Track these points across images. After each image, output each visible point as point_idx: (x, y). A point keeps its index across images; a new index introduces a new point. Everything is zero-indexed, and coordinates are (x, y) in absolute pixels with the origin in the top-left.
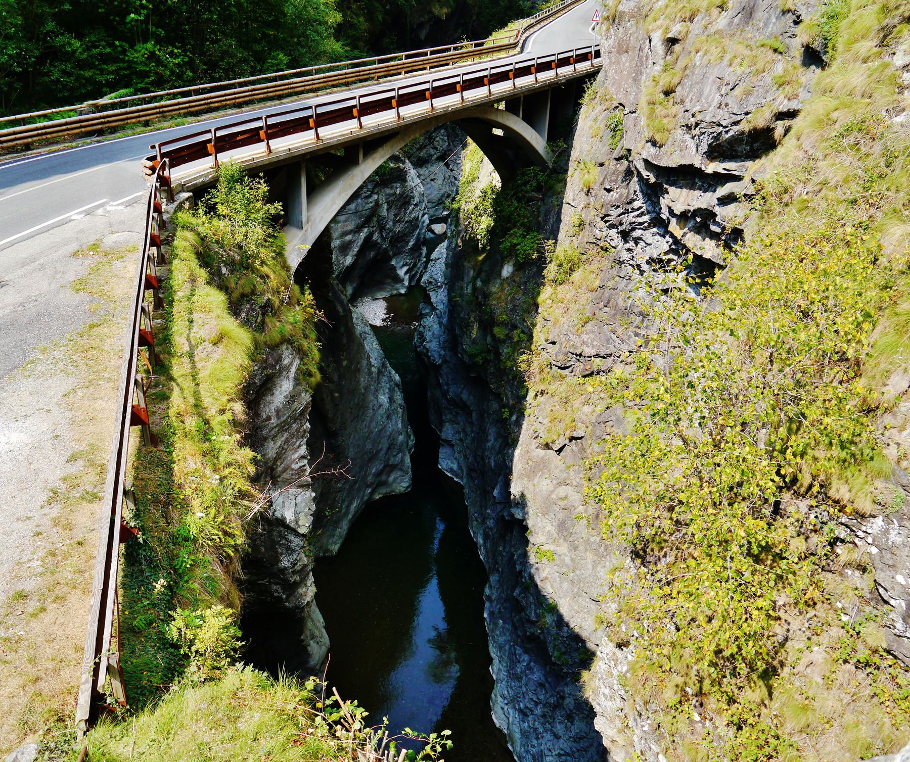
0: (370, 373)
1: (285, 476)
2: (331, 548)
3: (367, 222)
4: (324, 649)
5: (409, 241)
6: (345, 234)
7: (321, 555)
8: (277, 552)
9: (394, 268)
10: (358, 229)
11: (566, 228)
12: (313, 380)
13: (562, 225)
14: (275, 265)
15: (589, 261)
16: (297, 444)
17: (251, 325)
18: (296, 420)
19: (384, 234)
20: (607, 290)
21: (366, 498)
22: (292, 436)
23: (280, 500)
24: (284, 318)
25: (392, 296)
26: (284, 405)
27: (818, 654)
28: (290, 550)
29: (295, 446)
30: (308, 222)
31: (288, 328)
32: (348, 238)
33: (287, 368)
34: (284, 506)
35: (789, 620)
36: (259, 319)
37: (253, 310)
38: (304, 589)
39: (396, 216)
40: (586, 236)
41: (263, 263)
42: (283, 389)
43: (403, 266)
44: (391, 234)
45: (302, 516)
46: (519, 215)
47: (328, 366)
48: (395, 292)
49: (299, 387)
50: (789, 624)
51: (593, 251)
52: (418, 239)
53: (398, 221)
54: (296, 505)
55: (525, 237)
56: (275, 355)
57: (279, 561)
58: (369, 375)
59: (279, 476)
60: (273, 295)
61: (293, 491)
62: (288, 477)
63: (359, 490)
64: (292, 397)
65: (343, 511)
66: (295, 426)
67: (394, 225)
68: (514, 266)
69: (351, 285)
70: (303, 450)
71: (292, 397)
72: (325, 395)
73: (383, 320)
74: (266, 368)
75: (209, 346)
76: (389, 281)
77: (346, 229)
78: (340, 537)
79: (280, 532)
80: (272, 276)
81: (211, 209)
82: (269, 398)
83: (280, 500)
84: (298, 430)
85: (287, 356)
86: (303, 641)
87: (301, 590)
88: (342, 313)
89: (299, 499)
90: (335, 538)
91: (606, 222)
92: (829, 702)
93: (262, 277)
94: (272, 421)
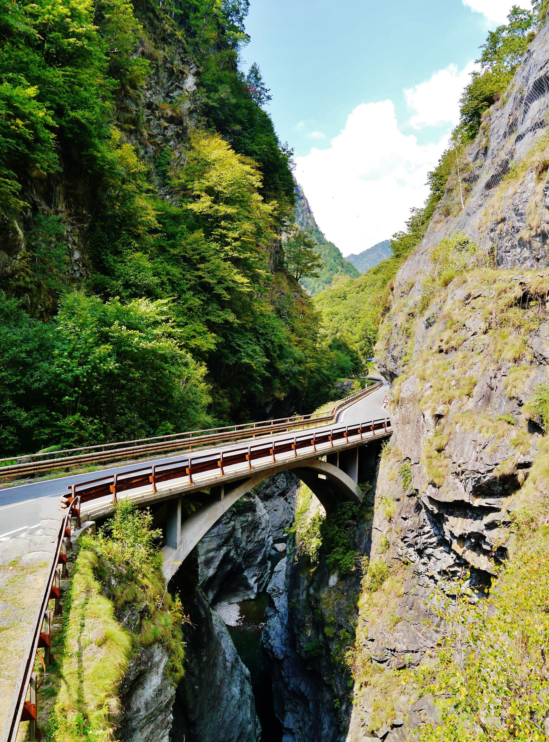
0: (225, 667)
3: (226, 542)
5: (257, 557)
6: (209, 551)
9: (246, 578)
10: (219, 548)
11: (376, 547)
13: (372, 545)
14: (154, 578)
15: (395, 573)
17: (131, 627)
18: (161, 711)
19: (239, 552)
20: (411, 596)
24: (157, 621)
25: (244, 601)
26: (152, 698)
30: (181, 543)
31: (161, 629)
32: (212, 554)
39: (248, 537)
40: (391, 553)
42: (153, 683)
43: (253, 576)
44: (244, 551)
48: (246, 598)
49: (166, 682)
51: (397, 565)
52: (265, 554)
53: (249, 541)
56: (148, 653)
60: (150, 602)
67: (246, 545)
68: (338, 576)
72: (187, 688)
73: (237, 621)
75: (94, 646)
76: (242, 588)
81: (108, 534)
82: (140, 692)
88: (204, 616)
91: (405, 542)
93: (142, 587)
94: (141, 713)
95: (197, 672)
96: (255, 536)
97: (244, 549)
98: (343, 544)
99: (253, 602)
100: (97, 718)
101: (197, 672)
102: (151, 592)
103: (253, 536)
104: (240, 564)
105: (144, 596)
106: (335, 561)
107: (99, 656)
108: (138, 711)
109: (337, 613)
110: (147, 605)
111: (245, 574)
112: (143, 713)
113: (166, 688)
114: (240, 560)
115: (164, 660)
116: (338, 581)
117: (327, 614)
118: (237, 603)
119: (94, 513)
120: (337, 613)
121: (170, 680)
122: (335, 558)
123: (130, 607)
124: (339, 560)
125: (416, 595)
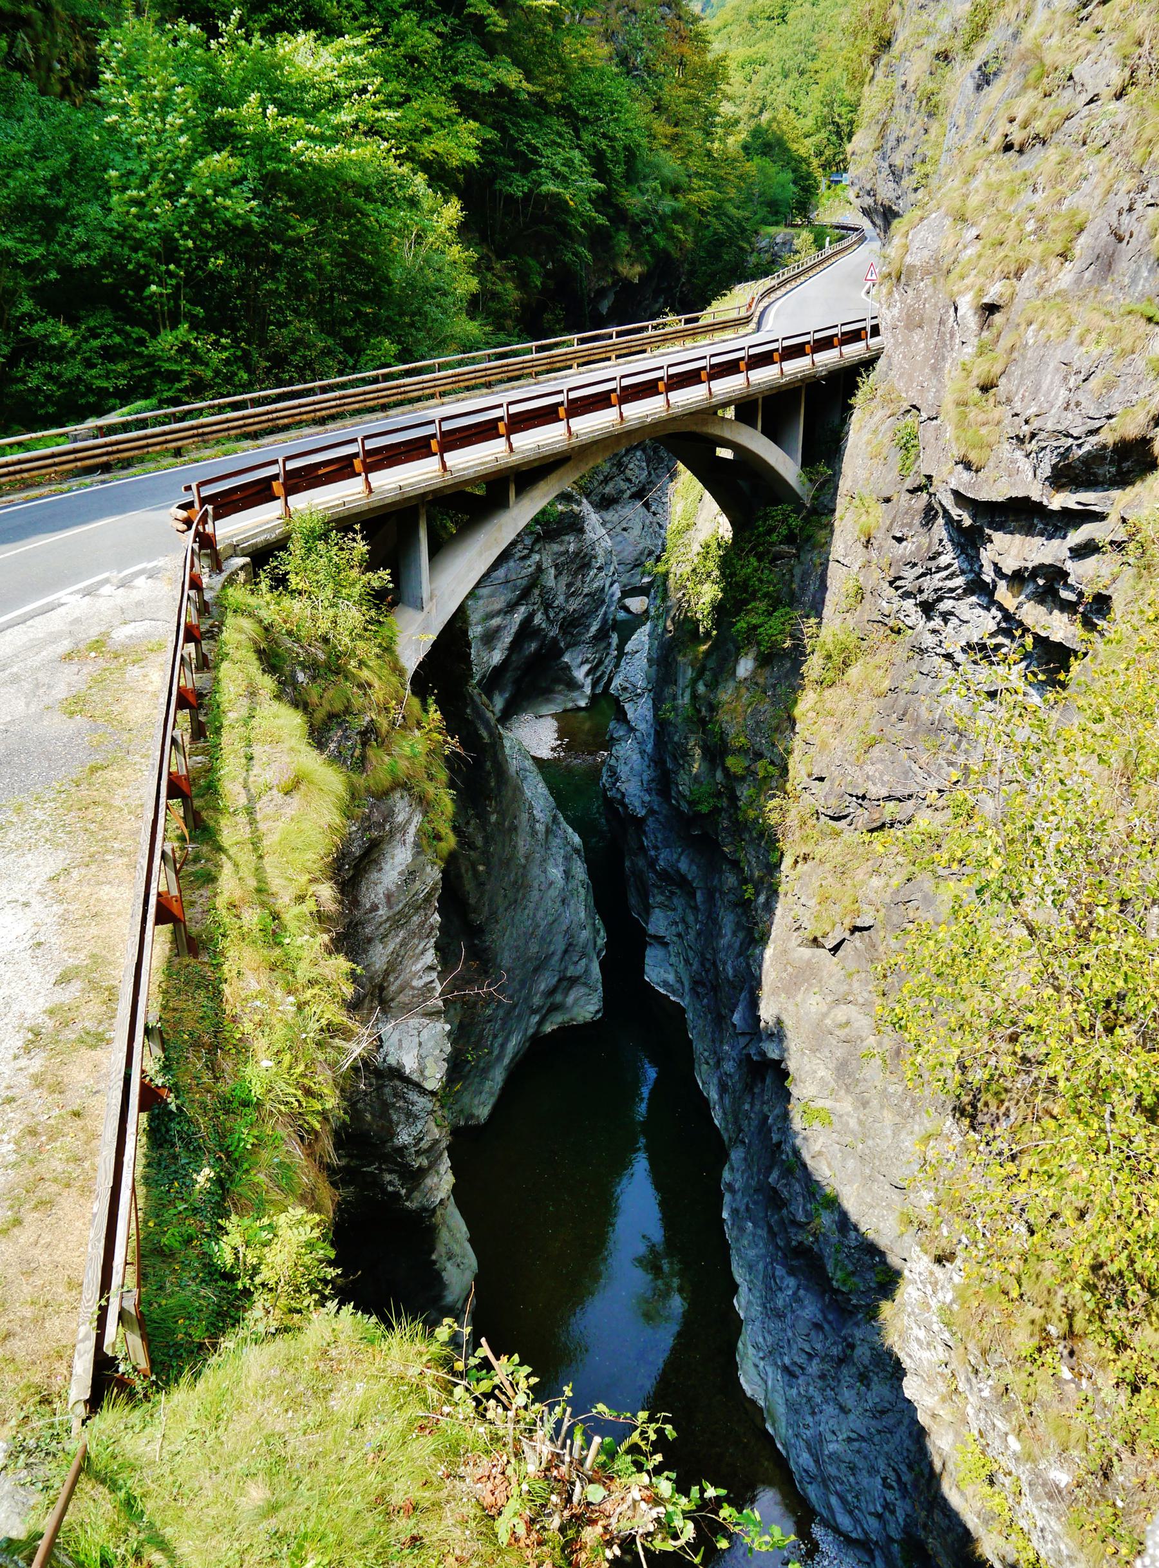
0: (534, 833)
1: (402, 998)
2: (476, 1112)
5: (590, 626)
7: (462, 1123)
8: (391, 1121)
9: (568, 668)
10: (511, 608)
13: (828, 596)
14: (381, 667)
15: (873, 651)
16: (421, 947)
17: (345, 762)
19: (552, 615)
20: (902, 695)
21: (531, 1031)
23: (395, 1037)
24: (396, 750)
25: (565, 711)
26: (398, 886)
30: (431, 599)
31: (403, 764)
32: (495, 622)
33: (403, 829)
34: (400, 1046)
36: (357, 753)
37: (348, 738)
38: (436, 1180)
39: (569, 585)
40: (867, 610)
41: (362, 664)
42: (397, 860)
43: (583, 663)
44: (562, 615)
45: (429, 1062)
46: (760, 580)
47: (468, 823)
48: (570, 705)
49: (422, 858)
53: (573, 594)
54: (420, 1044)
55: (770, 614)
56: (383, 807)
57: (393, 1135)
59: (392, 1000)
61: (414, 1022)
64: (411, 873)
65: (496, 1053)
67: (567, 601)
68: (756, 659)
72: (463, 870)
73: (553, 749)
74: (369, 828)
76: (561, 687)
77: (489, 609)
78: (492, 1094)
79: (394, 1088)
80: (376, 683)
81: (280, 581)
82: (374, 876)
83: (395, 1037)
84: (422, 925)
85: (403, 810)
89: (425, 1034)
90: (484, 1096)
91: (897, 588)
93: (360, 686)
94: (380, 912)
95: (479, 842)
97: (562, 610)
98: (766, 595)
99: (582, 714)
101: (479, 842)
103: (579, 584)
107: (289, 812)
108: (374, 908)
111: (566, 658)
112: (382, 912)
113: (424, 869)
114: (554, 632)
116: (756, 668)
117: (732, 732)
118: (552, 715)
119: (246, 540)
124: (756, 627)
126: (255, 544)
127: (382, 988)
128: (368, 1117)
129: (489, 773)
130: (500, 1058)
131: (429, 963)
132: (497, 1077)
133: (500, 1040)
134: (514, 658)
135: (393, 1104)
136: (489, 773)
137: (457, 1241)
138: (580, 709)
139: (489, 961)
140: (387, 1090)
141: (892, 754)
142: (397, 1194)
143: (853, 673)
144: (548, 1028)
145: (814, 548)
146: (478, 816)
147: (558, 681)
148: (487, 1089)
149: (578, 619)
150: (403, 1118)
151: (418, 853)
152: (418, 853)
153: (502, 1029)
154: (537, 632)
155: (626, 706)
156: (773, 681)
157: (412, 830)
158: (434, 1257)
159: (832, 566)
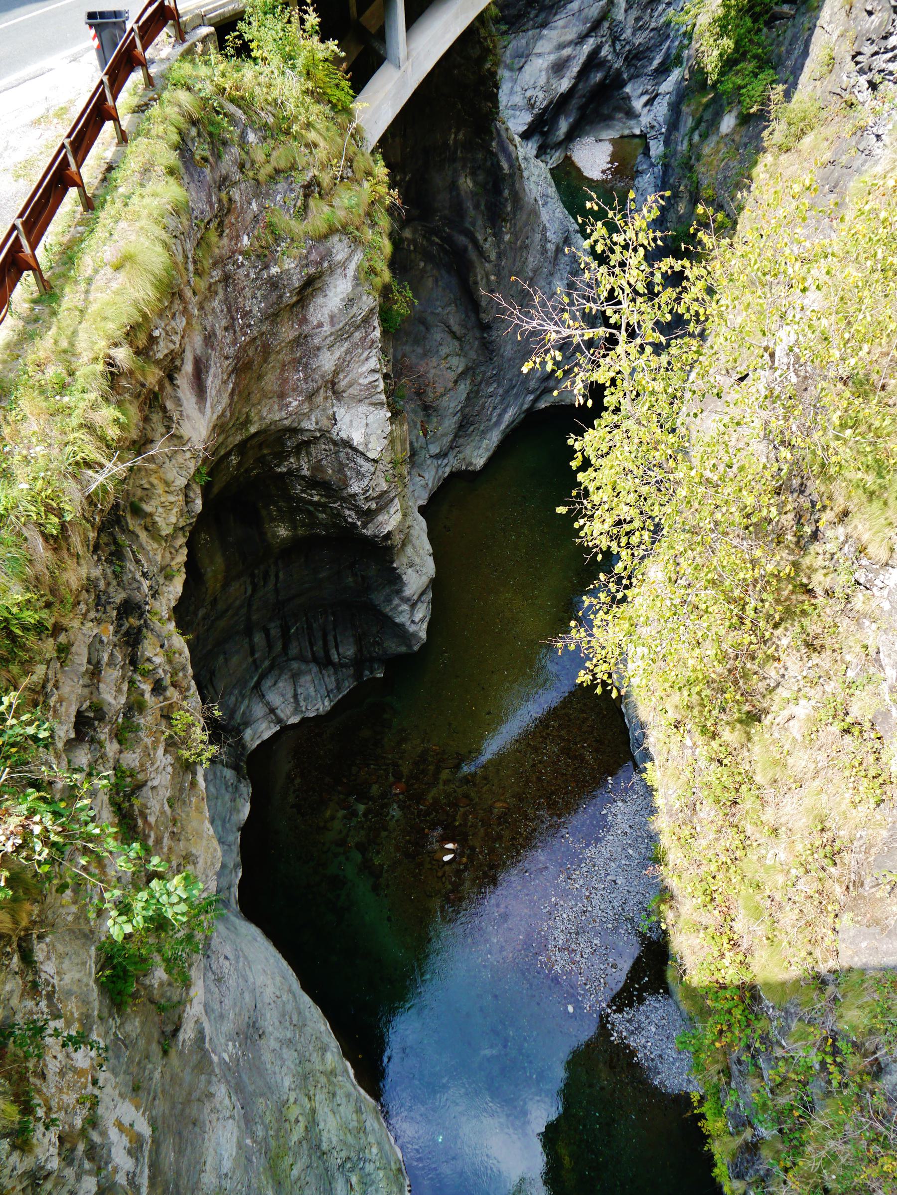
0: (544, 251)
1: (351, 391)
2: (474, 461)
3: (596, 26)
4: (424, 580)
5: (653, 59)
6: (561, 46)
7: (464, 468)
8: (345, 476)
9: (628, 98)
10: (582, 39)
11: (813, 66)
12: (378, 281)
13: (808, 63)
14: (328, 129)
15: (825, 122)
16: (365, 355)
17: (288, 210)
18: (358, 327)
19: (618, 48)
20: (838, 168)
21: (525, 407)
22: (355, 346)
23: (347, 418)
24: (336, 202)
25: (622, 137)
26: (340, 310)
27: (803, 710)
28: (360, 475)
29: (362, 358)
30: (408, 58)
31: (341, 214)
32: (567, 52)
33: (344, 265)
34: (351, 425)
35: (788, 664)
36: (299, 203)
37: (292, 190)
38: (386, 517)
39: (638, 19)
40: (830, 83)
41: (308, 125)
42: (339, 290)
43: (642, 94)
44: (627, 48)
45: (373, 438)
46: (751, 41)
47: (486, 240)
48: (626, 132)
49: (360, 288)
50: (786, 669)
51: (836, 105)
52: (667, 55)
53: (640, 28)
54: (367, 425)
55: (756, 75)
56: (321, 248)
57: (347, 486)
58: (542, 254)
59: (344, 391)
60: (320, 171)
61: (363, 408)
62: (356, 393)
63: (517, 396)
64: (350, 300)
65: (494, 420)
66: (358, 335)
67: (634, 34)
68: (737, 117)
69: (566, 119)
70: (373, 363)
71: (350, 300)
72: (479, 277)
73: (603, 172)
74: (307, 265)
75: (109, 270)
76: (621, 115)
77: (563, 39)
78: (487, 450)
79: (347, 454)
80: (322, 144)
81: (244, 50)
82: (320, 300)
83: (347, 418)
84: (363, 339)
85: (340, 249)
86: (396, 569)
87: (381, 518)
88: (506, 171)
89: (371, 419)
90: (481, 451)
91: (857, 63)
92: (800, 761)
93: (307, 145)
94: (325, 329)
95: (493, 256)
96: (652, 17)
97: (628, 43)
98: (756, 57)
99: (637, 140)
100: (86, 377)
101: (493, 256)
102: (321, 154)
103: (647, 18)
104: (619, 72)
105: (311, 160)
106: (733, 88)
107: (115, 285)
108: (320, 325)
109: (720, 183)
110: (315, 176)
111: (628, 89)
112: (327, 329)
113: (361, 298)
114: (618, 64)
115: (356, 258)
116: (736, 125)
117: (705, 183)
118: (611, 140)
119: (215, 9)
120: (720, 183)
121: (366, 287)
122: (733, 83)
123: (287, 178)
124: (740, 87)
125: (847, 168)
126: (224, 13)
127: (333, 384)
128: (330, 471)
129: (507, 200)
130: (498, 423)
131: (372, 367)
132: (494, 438)
133: (498, 411)
134: (580, 86)
135: (347, 465)
136: (507, 200)
137: (419, 555)
138: (634, 136)
139: (493, 351)
140: (342, 455)
141: (818, 221)
142: (354, 525)
143: (807, 140)
144: (542, 405)
145: (808, 11)
146: (495, 235)
147: (618, 109)
148: (484, 446)
149: (643, 52)
150: (354, 475)
151: (358, 285)
152: (358, 285)
153: (502, 402)
154: (603, 63)
155: (652, 143)
156: (746, 140)
157: (352, 266)
158: (395, 565)
159: (818, 31)
